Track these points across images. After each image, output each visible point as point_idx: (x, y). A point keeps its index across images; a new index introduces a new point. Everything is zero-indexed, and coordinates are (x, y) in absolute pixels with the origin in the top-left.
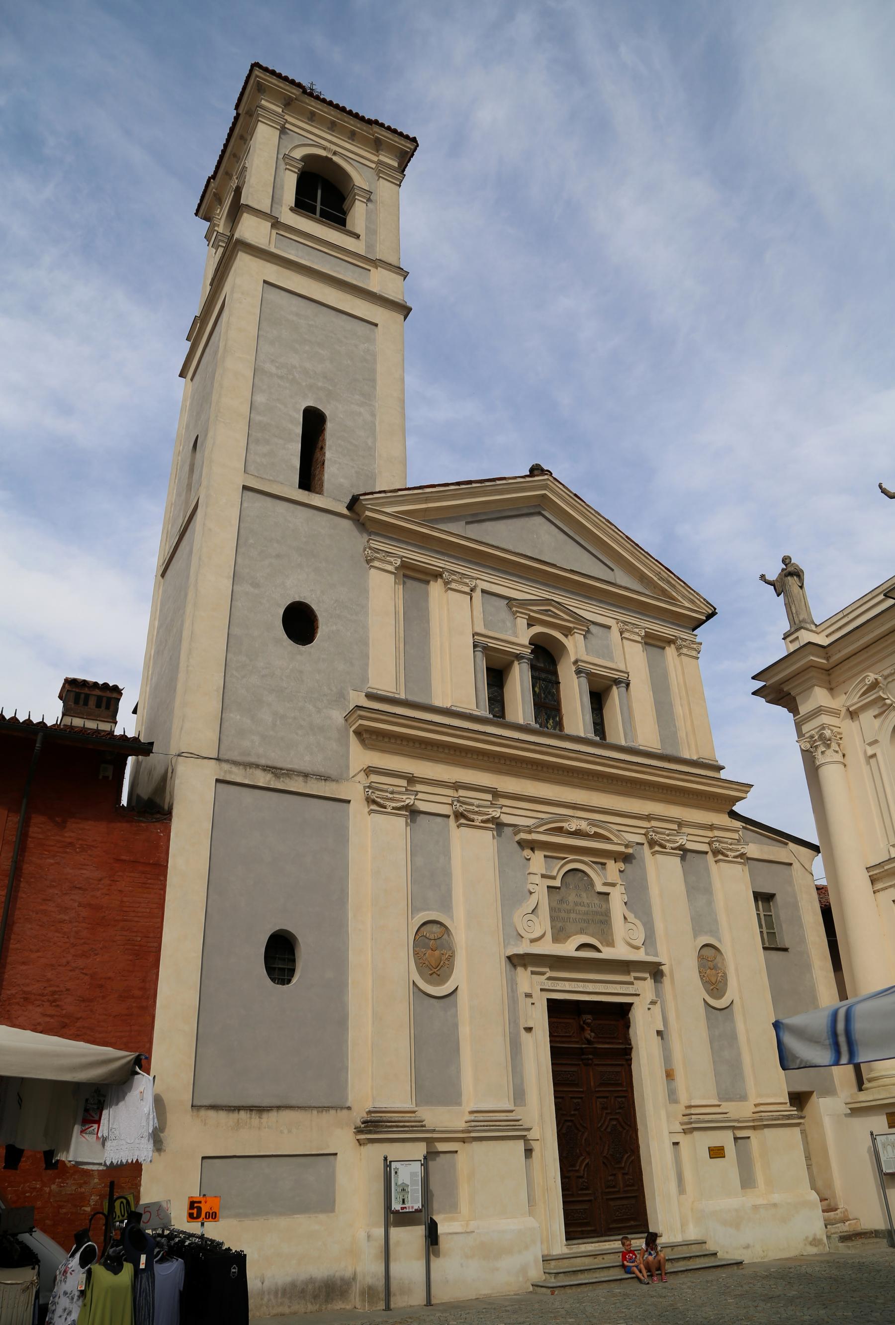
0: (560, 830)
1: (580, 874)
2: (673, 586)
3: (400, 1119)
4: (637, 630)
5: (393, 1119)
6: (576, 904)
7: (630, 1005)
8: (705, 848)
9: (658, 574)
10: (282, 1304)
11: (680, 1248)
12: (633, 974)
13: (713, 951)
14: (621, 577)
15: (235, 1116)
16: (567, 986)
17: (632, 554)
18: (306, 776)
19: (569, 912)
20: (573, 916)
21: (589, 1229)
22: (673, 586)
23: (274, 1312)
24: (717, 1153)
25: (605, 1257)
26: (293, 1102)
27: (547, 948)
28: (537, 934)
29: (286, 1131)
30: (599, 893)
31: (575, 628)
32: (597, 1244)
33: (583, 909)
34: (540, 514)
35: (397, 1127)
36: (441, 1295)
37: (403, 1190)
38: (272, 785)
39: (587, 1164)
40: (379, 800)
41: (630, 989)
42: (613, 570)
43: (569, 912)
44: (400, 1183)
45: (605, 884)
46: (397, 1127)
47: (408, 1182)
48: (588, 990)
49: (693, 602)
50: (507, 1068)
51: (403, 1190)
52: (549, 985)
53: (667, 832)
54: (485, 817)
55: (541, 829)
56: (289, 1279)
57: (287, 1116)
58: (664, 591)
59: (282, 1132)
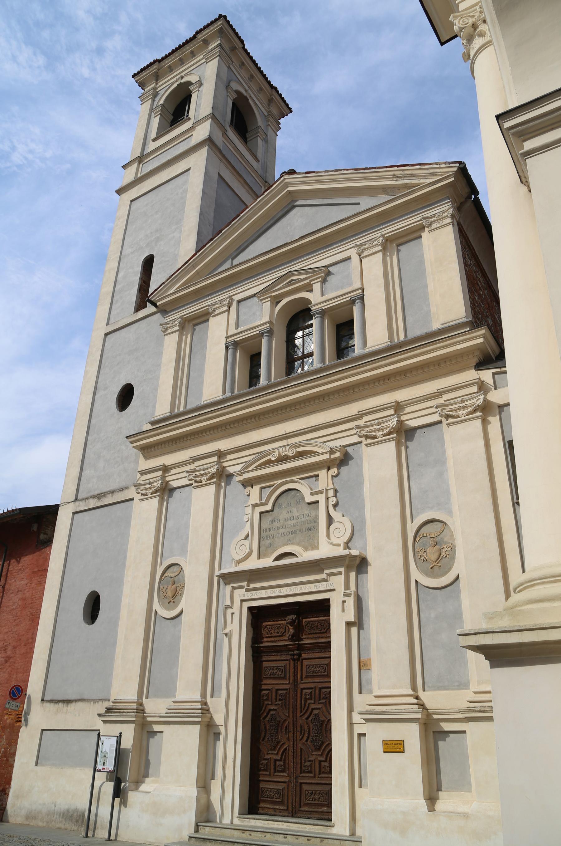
0: (269, 462)
1: (293, 492)
2: (411, 176)
3: (122, 707)
4: (376, 243)
5: (118, 708)
6: (286, 520)
7: (328, 600)
8: (436, 418)
9: (394, 177)
10: (61, 822)
11: (330, 841)
12: (326, 571)
13: (440, 525)
14: (366, 202)
15: (57, 706)
16: (264, 593)
17: (366, 179)
18: (113, 492)
19: (279, 528)
20: (282, 531)
21: (281, 808)
22: (411, 176)
23: (58, 826)
24: (394, 747)
25: (252, 833)
26: (86, 697)
27: (253, 563)
28: (242, 553)
29: (77, 715)
30: (310, 504)
31: (311, 281)
32: (266, 822)
33: (292, 522)
34: (295, 206)
35: (119, 712)
36: (124, 835)
37: (105, 756)
38: (100, 504)
39: (286, 749)
40: (451, 413)
41: (325, 586)
42: (359, 204)
43: (279, 528)
44: (103, 751)
45: (312, 494)
46: (119, 712)
47: (108, 751)
48: (282, 594)
49: (434, 174)
50: (211, 669)
51: (105, 756)
52: (249, 595)
53: (377, 421)
54: (470, 409)
55: (251, 468)
56: (66, 807)
57: (80, 704)
58: (407, 186)
59: (75, 716)
